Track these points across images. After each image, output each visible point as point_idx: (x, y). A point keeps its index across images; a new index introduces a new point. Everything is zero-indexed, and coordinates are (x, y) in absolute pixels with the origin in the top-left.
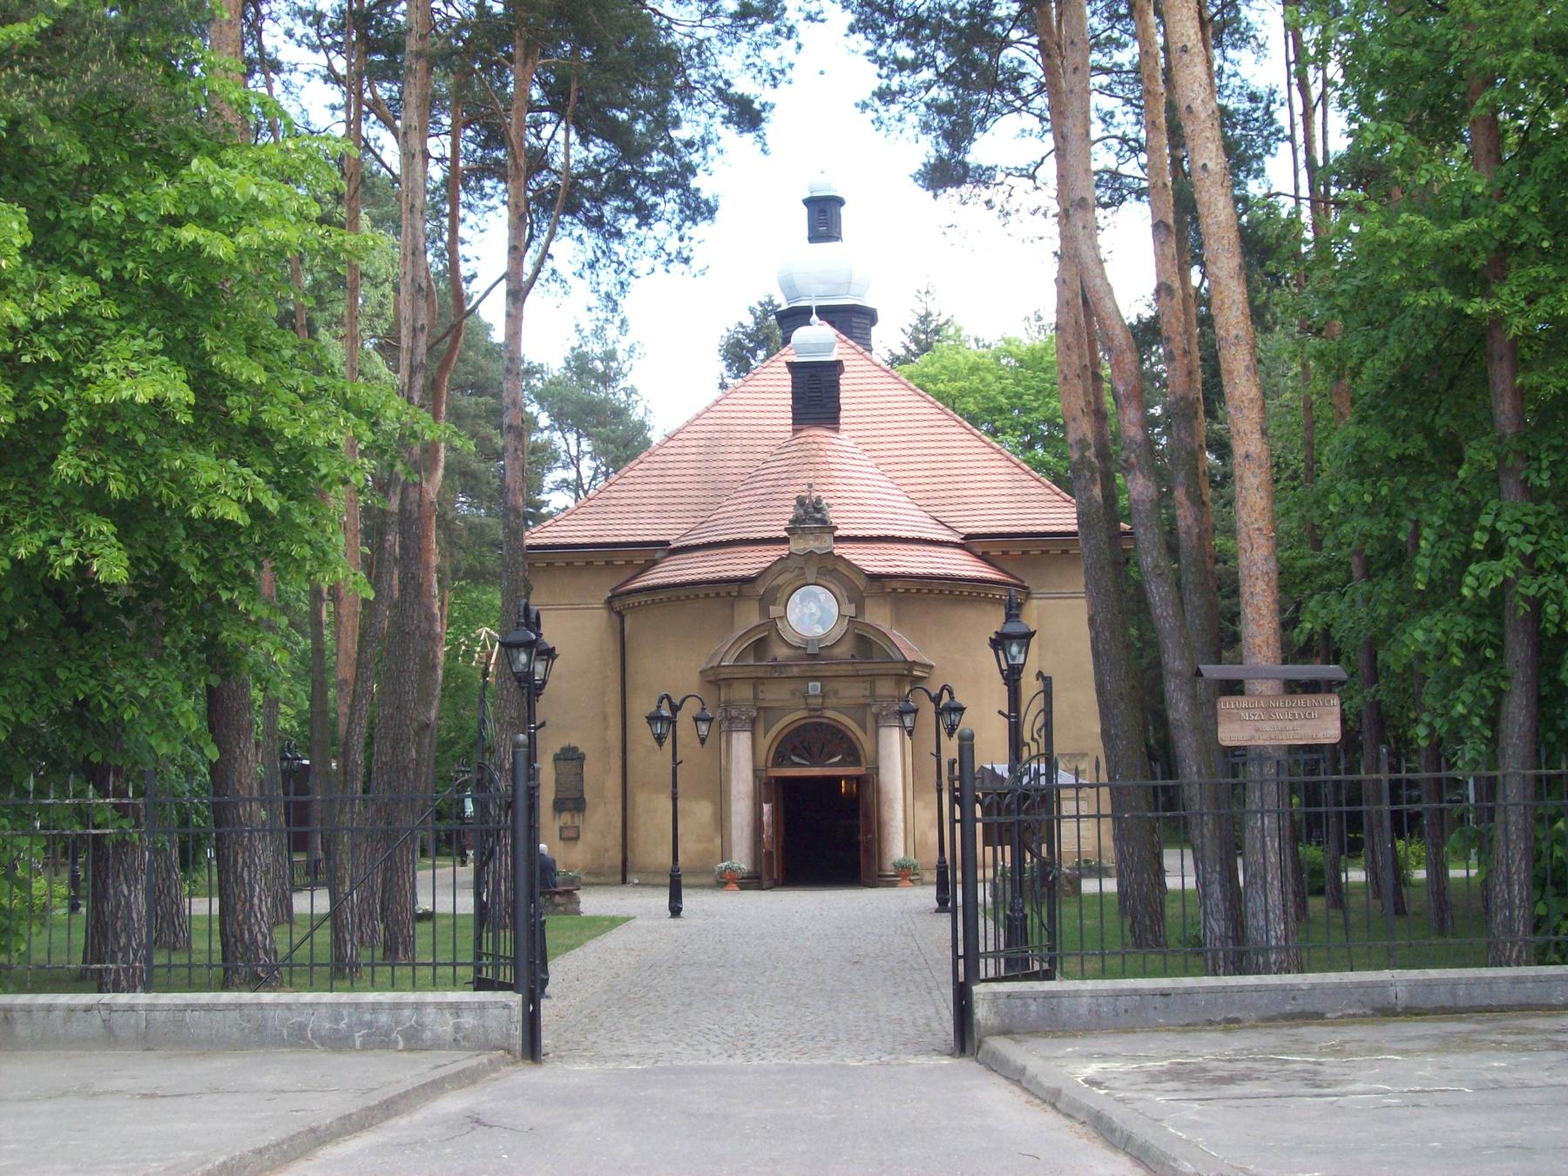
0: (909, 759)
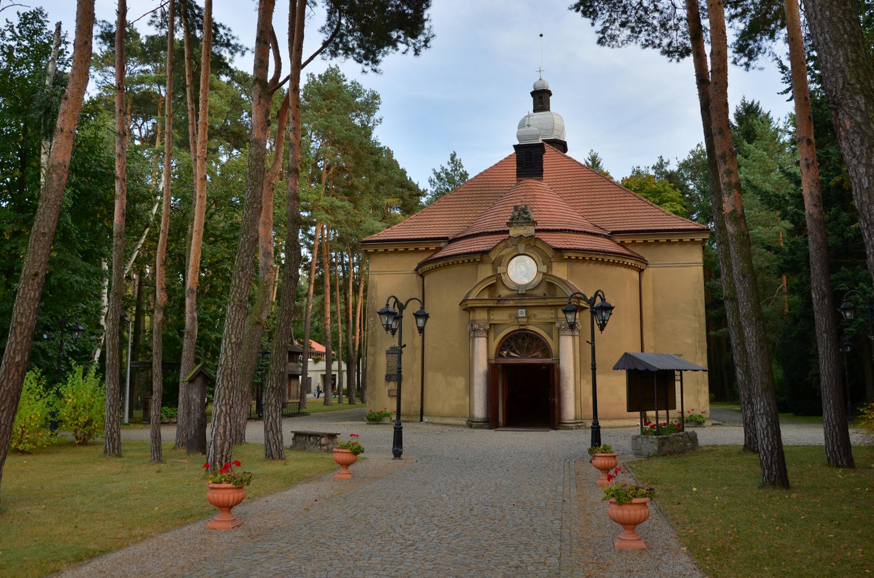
0: (578, 355)
